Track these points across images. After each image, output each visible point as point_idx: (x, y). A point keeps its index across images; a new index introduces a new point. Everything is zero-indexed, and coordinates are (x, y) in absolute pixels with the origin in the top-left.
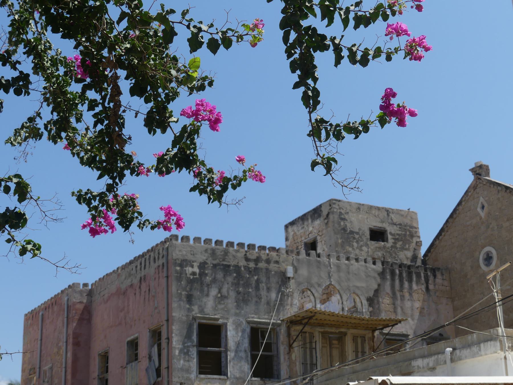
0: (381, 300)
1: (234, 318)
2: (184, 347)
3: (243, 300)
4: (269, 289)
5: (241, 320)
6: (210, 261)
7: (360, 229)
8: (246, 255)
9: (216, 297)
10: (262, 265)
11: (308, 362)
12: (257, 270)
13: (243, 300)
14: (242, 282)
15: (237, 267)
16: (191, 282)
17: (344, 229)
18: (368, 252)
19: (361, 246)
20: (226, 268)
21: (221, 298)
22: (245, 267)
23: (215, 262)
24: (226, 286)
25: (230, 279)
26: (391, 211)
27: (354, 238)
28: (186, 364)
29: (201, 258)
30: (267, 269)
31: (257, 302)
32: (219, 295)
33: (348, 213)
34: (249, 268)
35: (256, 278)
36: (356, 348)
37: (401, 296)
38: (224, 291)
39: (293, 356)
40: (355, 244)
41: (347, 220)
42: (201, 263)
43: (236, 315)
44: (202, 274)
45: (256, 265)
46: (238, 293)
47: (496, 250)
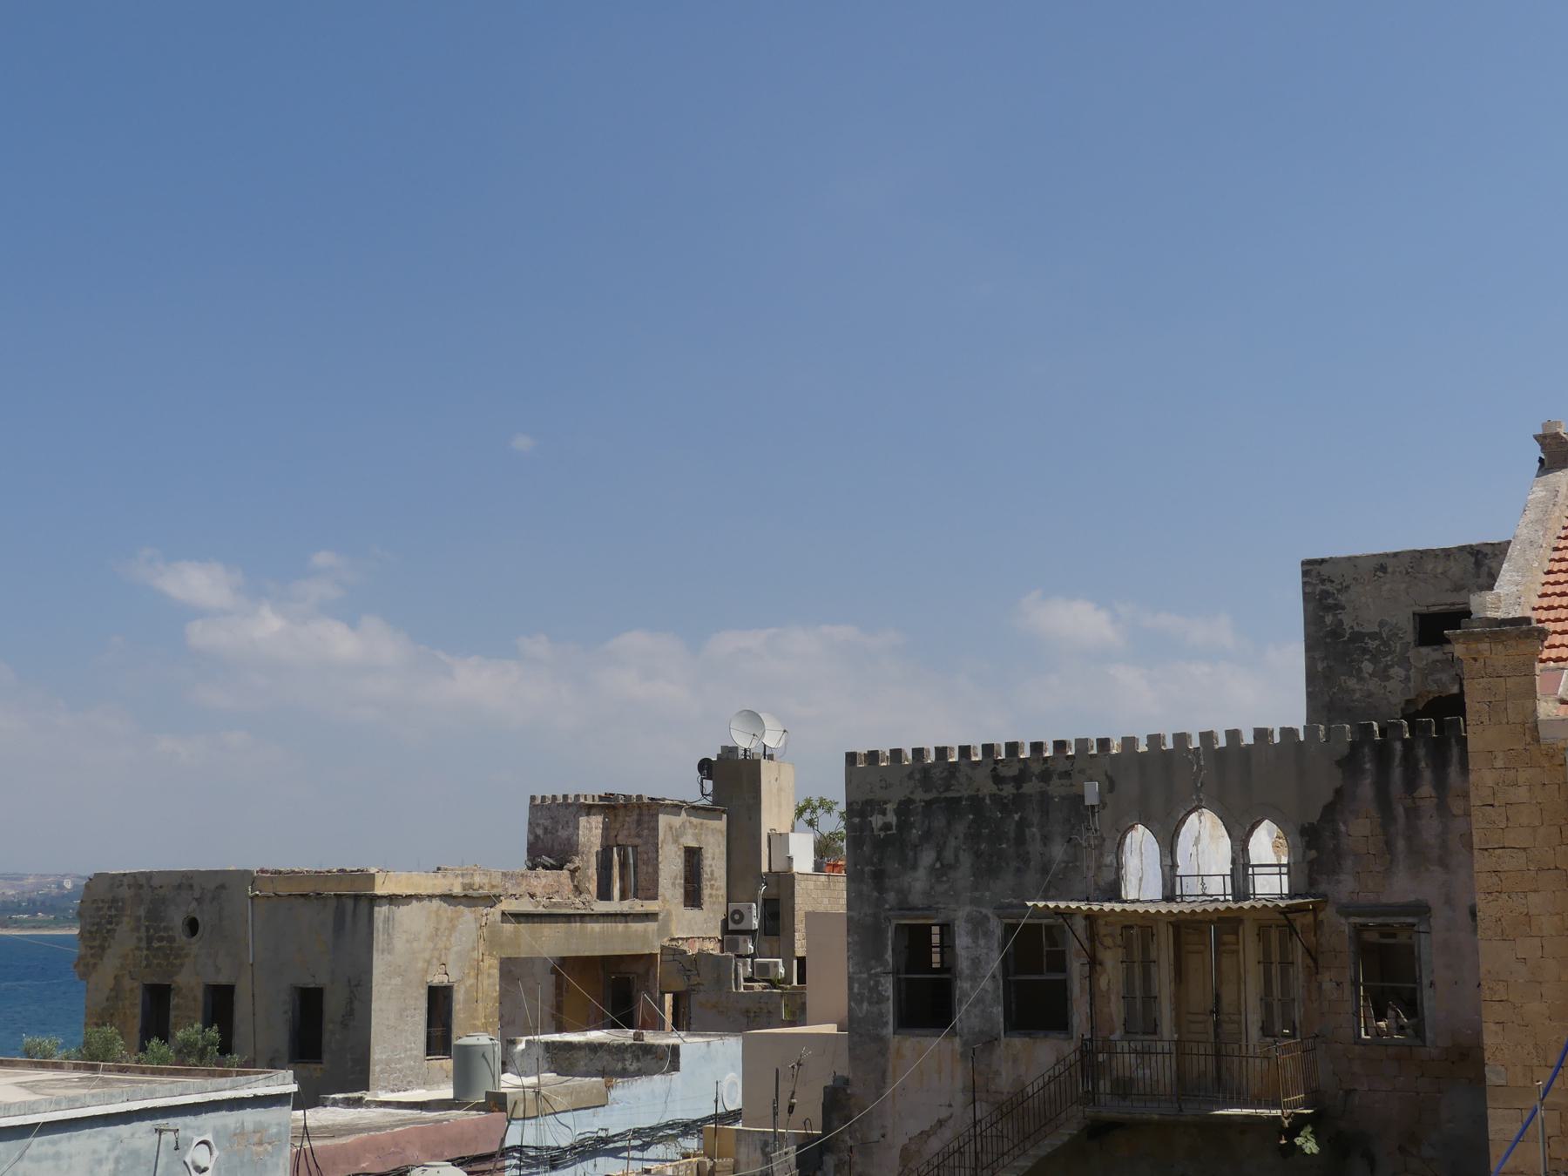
0: (1343, 828)
1: (968, 909)
2: (870, 976)
3: (987, 869)
4: (1046, 839)
5: (984, 911)
6: (920, 796)
7: (1382, 624)
8: (994, 769)
9: (932, 869)
10: (1032, 787)
11: (1138, 994)
12: (1019, 801)
13: (987, 869)
14: (986, 831)
15: (976, 802)
16: (881, 845)
17: (1336, 633)
18: (1408, 679)
19: (1387, 667)
20: (952, 806)
21: (942, 871)
22: (992, 796)
23: (928, 797)
24: (952, 843)
25: (960, 828)
26: (1485, 550)
27: (1365, 651)
28: (875, 1009)
29: (898, 794)
30: (1043, 794)
31: (1018, 870)
32: (938, 865)
33: (1348, 587)
34: (1002, 798)
35: (1017, 817)
36: (1267, 953)
37: (1406, 810)
38: (948, 855)
39: (1103, 982)
40: (1368, 667)
41: (1343, 608)
42: (900, 803)
43: (973, 901)
44: (904, 825)
45: (1019, 787)
46: (978, 855)
47: (1124, 837)
